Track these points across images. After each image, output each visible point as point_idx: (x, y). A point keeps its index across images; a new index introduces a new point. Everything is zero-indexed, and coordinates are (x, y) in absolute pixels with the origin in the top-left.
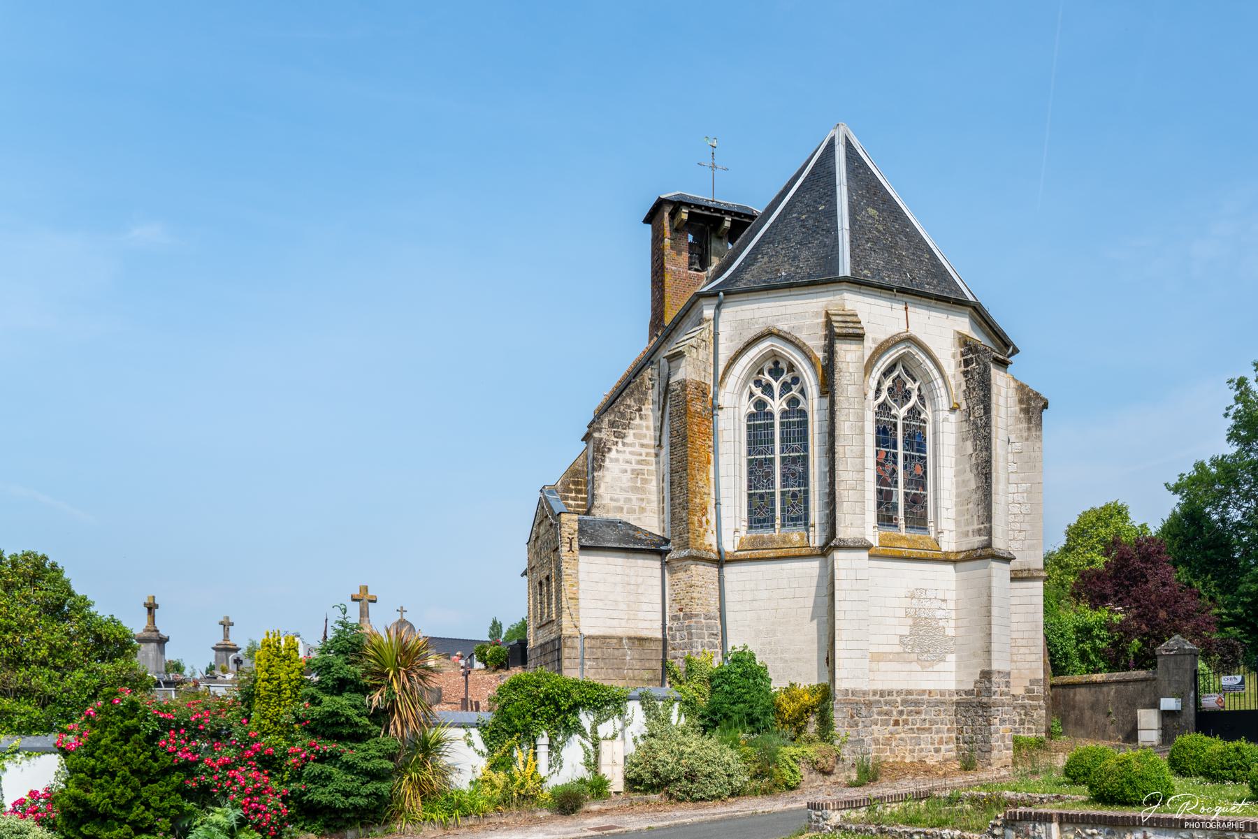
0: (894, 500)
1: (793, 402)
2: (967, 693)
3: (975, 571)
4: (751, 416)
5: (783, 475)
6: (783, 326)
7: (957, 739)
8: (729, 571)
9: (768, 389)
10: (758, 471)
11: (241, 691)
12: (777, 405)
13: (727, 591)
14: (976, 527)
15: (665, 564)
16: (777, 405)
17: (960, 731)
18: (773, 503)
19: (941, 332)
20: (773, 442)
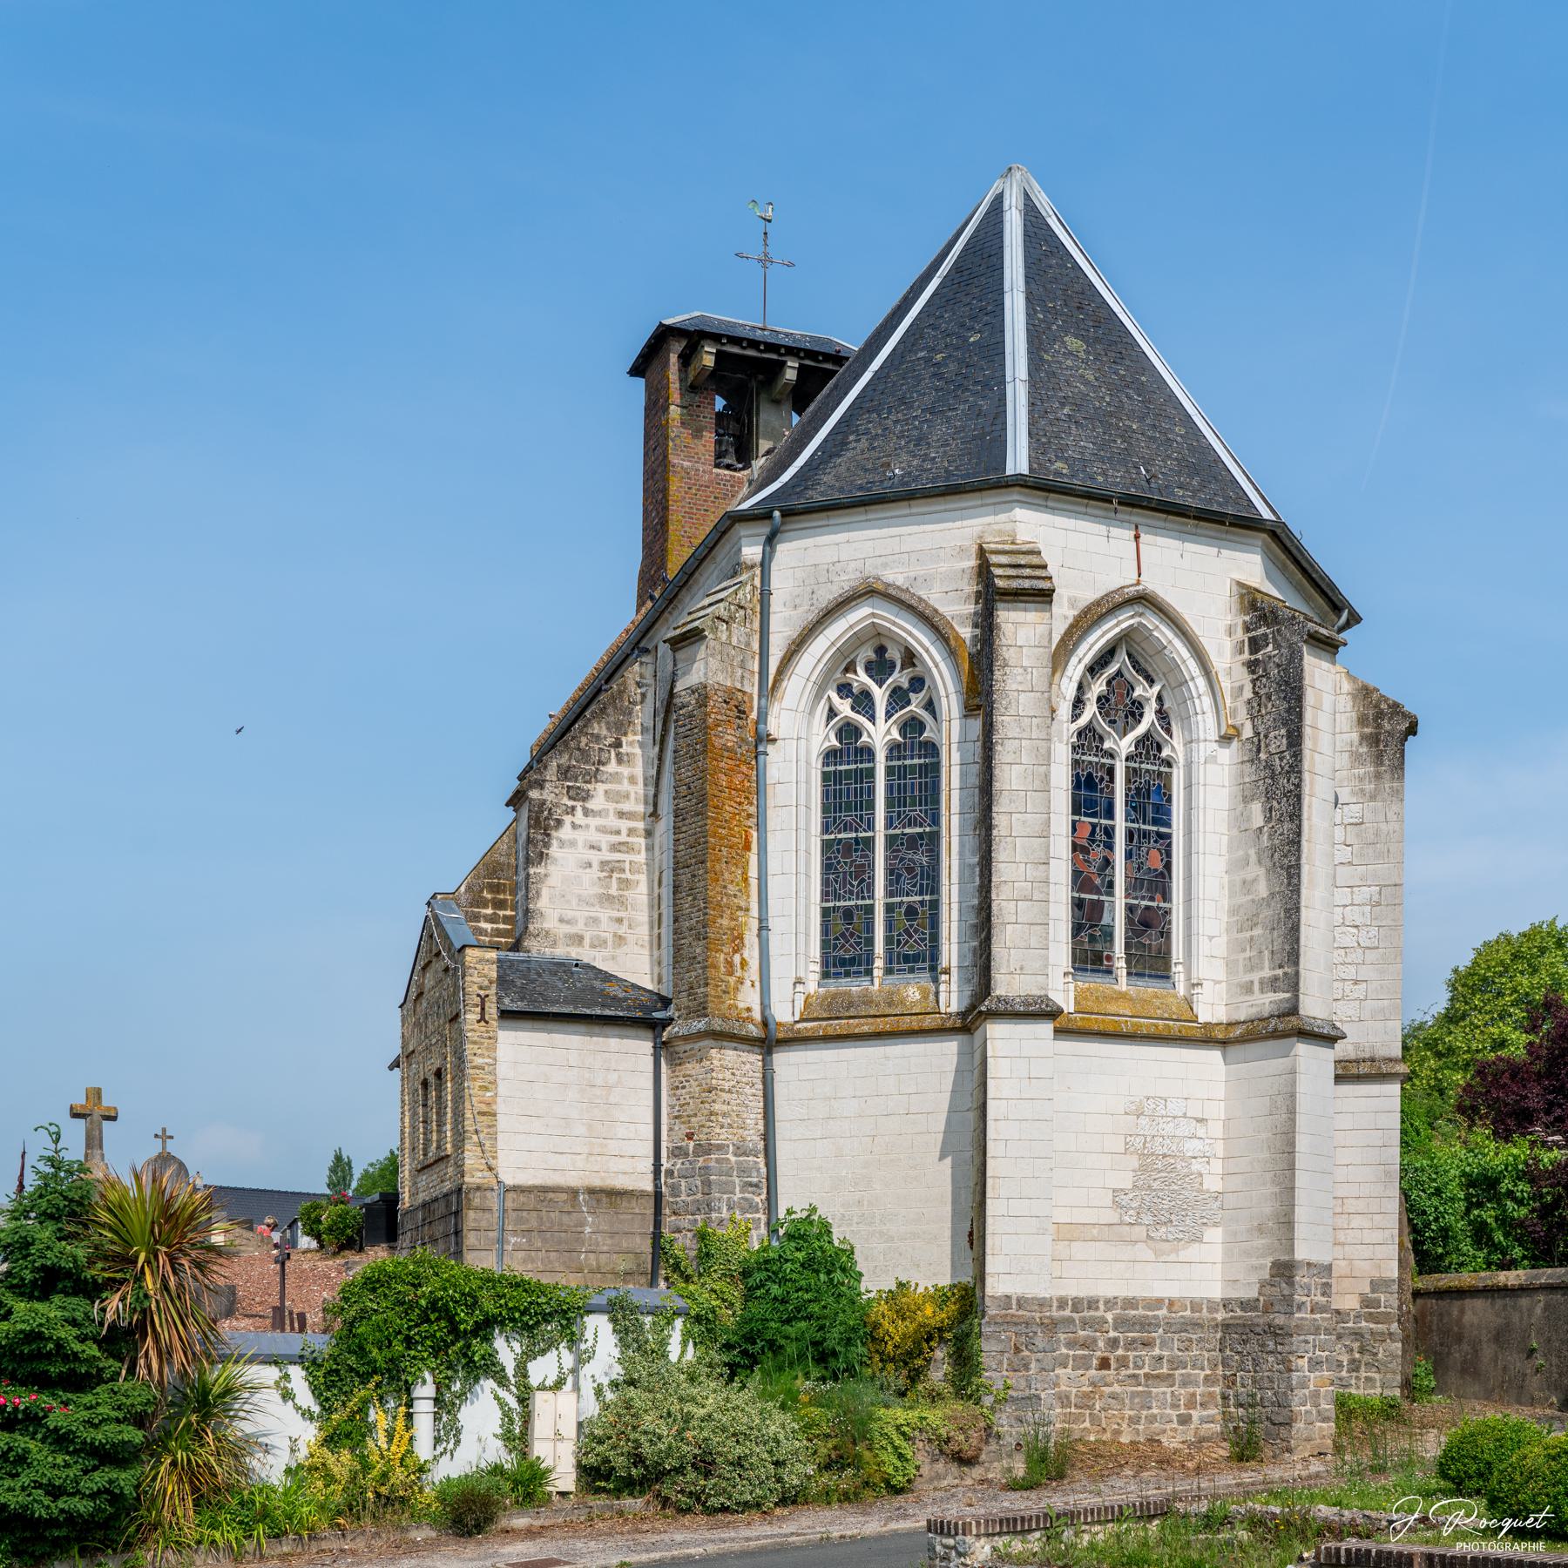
0: (1106, 920)
1: (912, 726)
2: (1245, 1305)
6: (895, 576)
7: (1225, 1398)
9: (863, 702)
10: (843, 864)
12: (880, 733)
13: (651, 1075)
14: (1267, 973)
16: (880, 733)
17: (1230, 1381)
18: (870, 927)
20: (871, 805)
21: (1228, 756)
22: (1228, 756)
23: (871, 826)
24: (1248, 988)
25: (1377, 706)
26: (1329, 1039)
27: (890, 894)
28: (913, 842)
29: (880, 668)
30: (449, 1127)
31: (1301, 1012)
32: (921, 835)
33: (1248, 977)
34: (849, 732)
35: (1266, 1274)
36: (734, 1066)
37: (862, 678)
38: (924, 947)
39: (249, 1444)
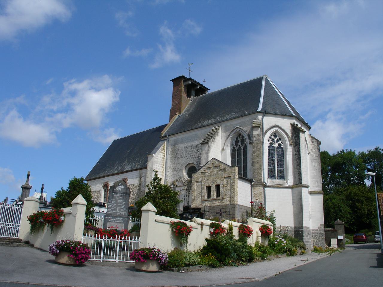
0: (374, 204)
1: (280, 145)
2: (316, 230)
3: (297, 190)
4: (269, 147)
5: (277, 164)
6: (280, 125)
7: (313, 243)
8: (266, 189)
9: (273, 140)
10: (271, 162)
11: (126, 208)
12: (276, 145)
13: (250, 191)
14: (317, 185)
15: (252, 186)
16: (276, 145)
17: (314, 241)
18: (275, 171)
19: (286, 124)
20: (274, 154)
21: (309, 156)
22: (308, 156)
23: (274, 157)
24: (314, 187)
25: (352, 158)
26: (307, 187)
27: (277, 167)
28: (280, 160)
29: (275, 136)
30: (244, 224)
31: (302, 183)
32: (281, 160)
33: (314, 185)
34: (271, 144)
35: (319, 226)
36: (260, 189)
37: (273, 137)
38: (283, 175)
39: (179, 200)
